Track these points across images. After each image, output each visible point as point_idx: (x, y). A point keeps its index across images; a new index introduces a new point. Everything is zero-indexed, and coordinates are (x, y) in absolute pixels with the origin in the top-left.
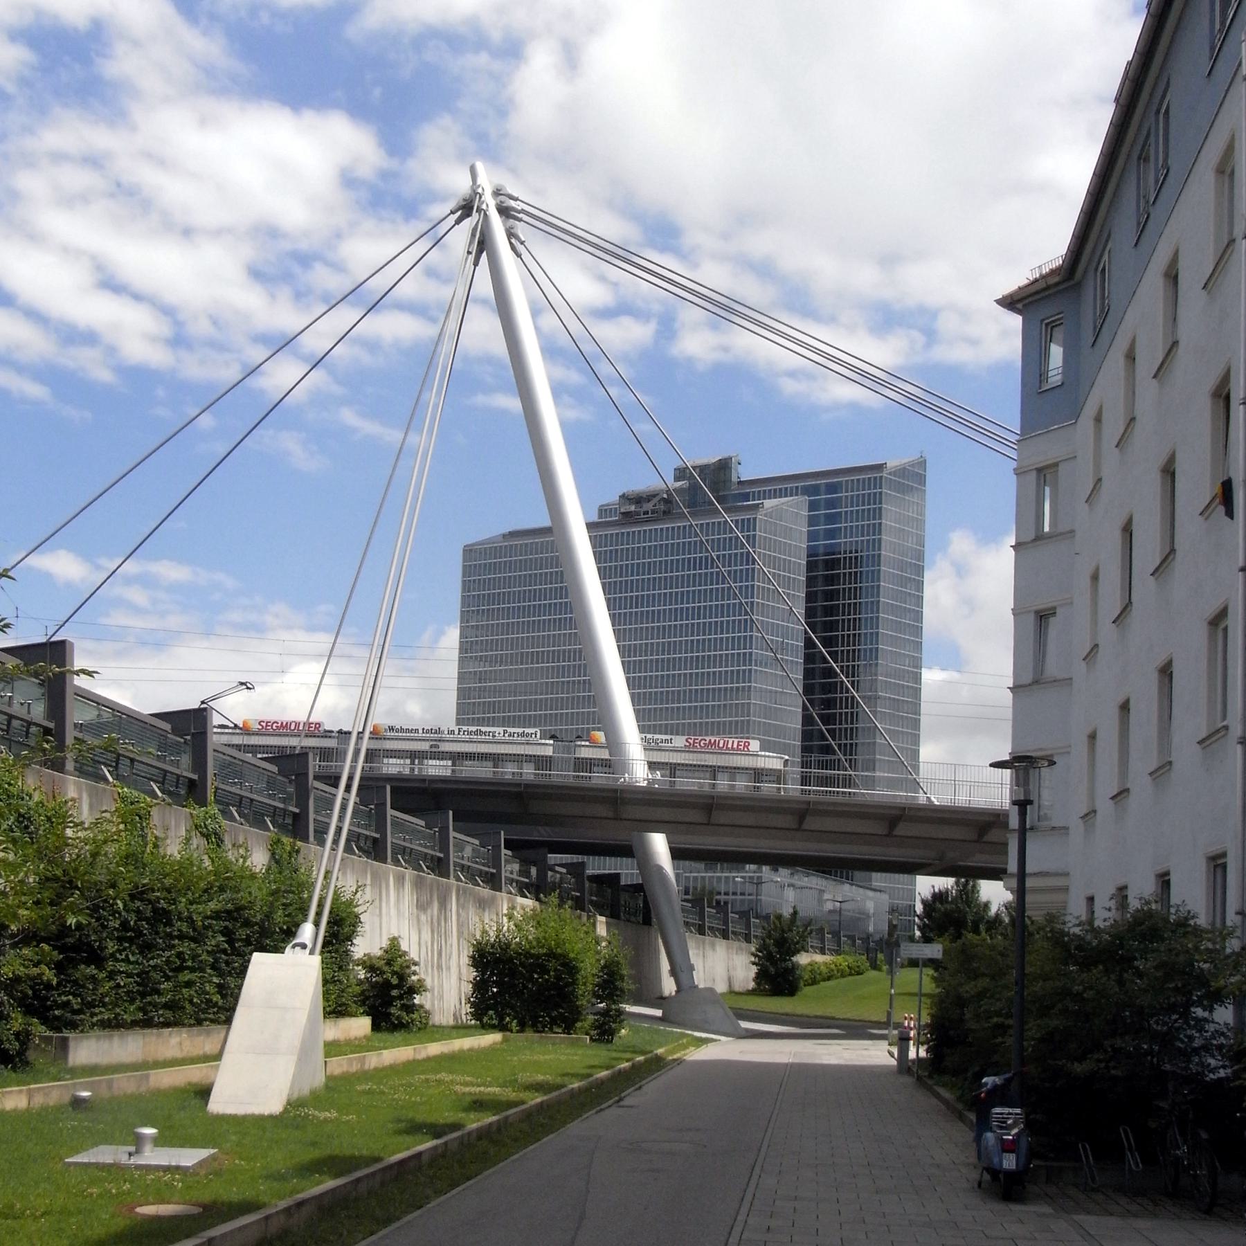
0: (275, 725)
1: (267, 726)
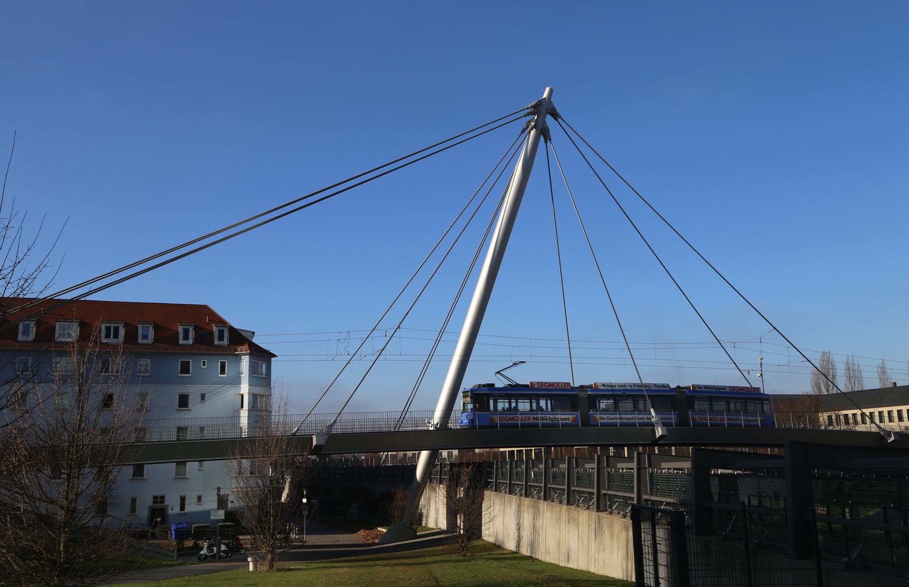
0: (737, 389)
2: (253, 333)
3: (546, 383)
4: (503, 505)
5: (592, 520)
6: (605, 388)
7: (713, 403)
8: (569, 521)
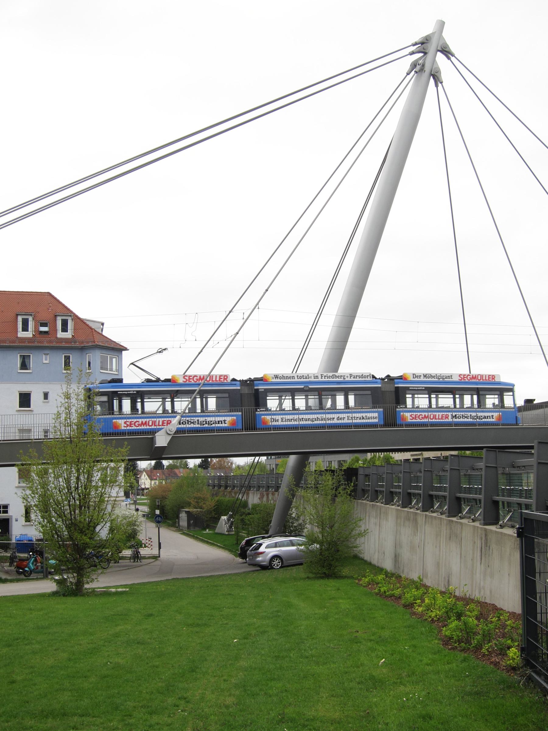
0: (195, 378)
1: (190, 379)
2: (103, 324)
3: (196, 376)
4: (379, 518)
5: (477, 536)
6: (428, 379)
7: (323, 397)
8: (450, 537)
